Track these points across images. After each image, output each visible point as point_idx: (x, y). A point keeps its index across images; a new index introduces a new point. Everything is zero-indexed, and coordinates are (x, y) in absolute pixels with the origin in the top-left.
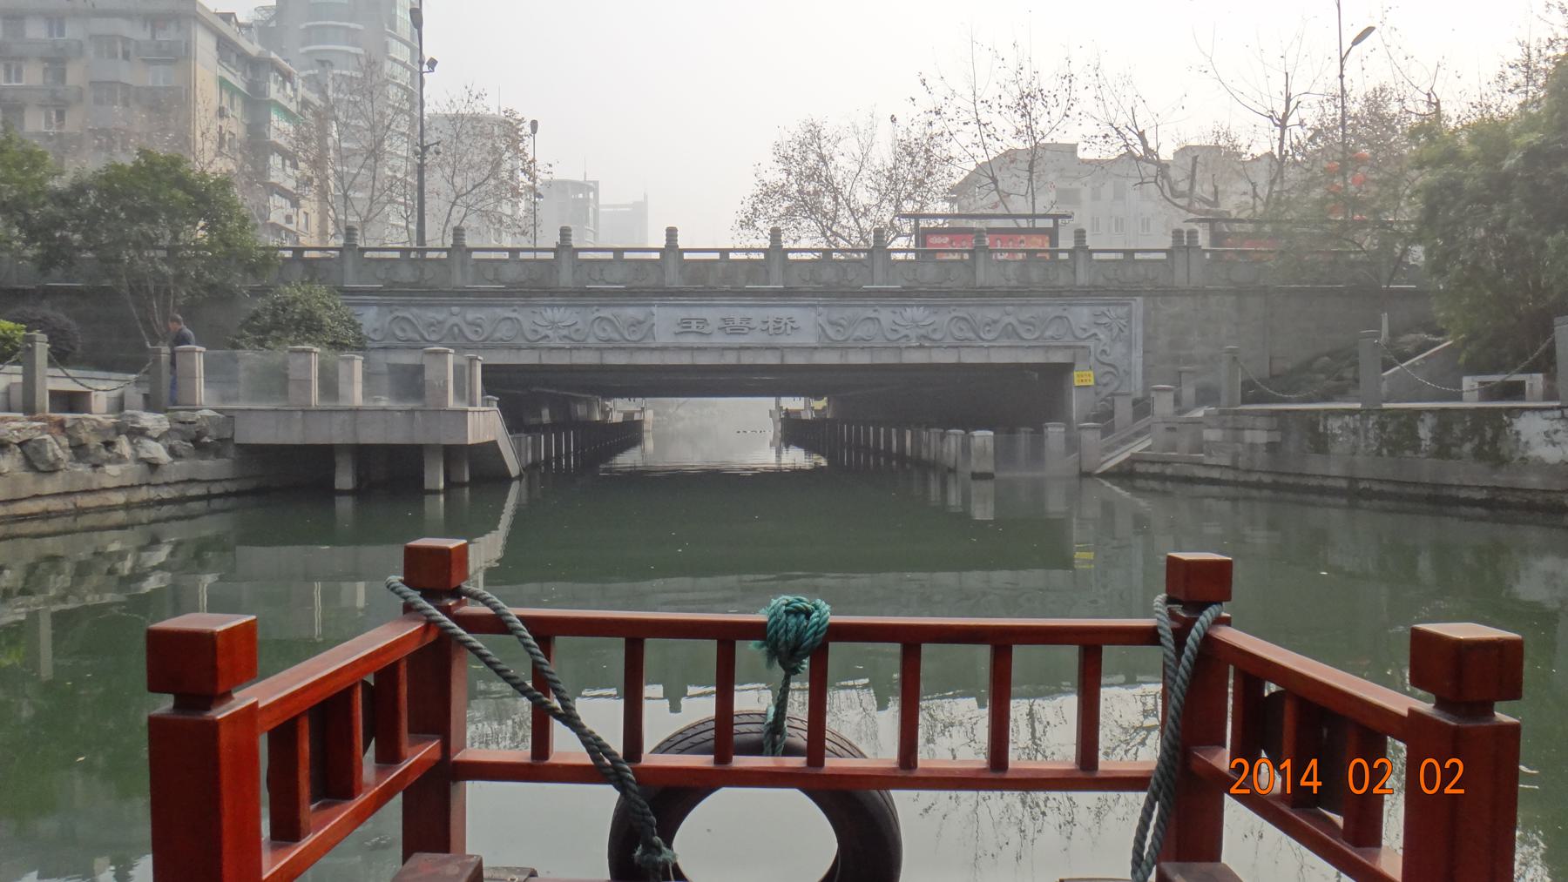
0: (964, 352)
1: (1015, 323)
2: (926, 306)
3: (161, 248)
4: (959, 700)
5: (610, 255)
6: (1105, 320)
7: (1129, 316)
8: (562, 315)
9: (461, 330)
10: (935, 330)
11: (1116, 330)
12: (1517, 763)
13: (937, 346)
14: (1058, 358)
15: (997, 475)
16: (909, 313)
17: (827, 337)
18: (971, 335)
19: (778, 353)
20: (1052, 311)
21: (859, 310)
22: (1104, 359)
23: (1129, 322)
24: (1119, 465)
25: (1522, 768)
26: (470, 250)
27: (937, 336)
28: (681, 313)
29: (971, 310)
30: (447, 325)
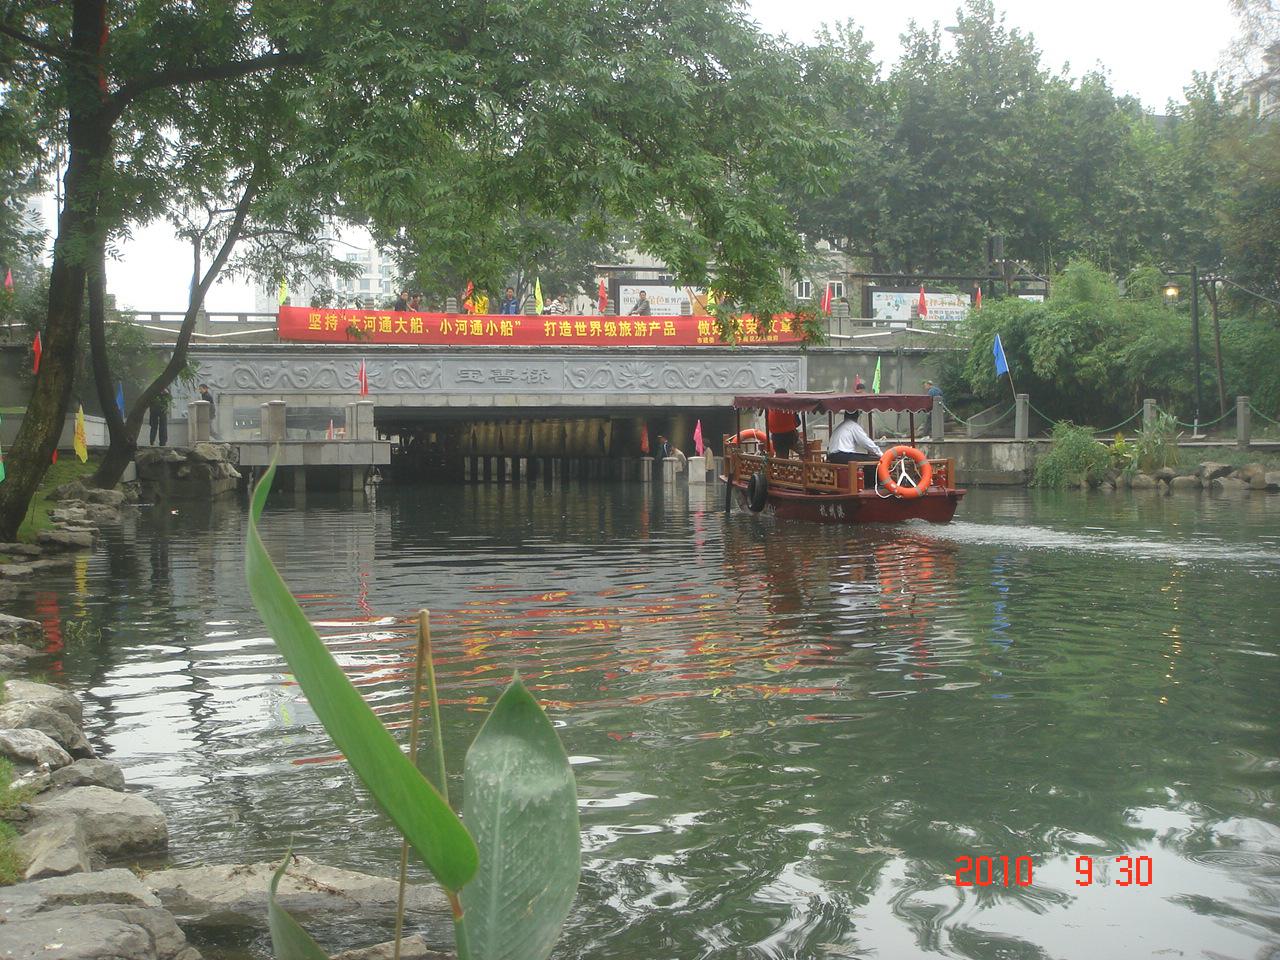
1: (712, 375)
3: (467, 298)
5: (235, 319)
9: (289, 379)
12: (310, 700)
21: (596, 364)
25: (305, 700)
26: (208, 315)
28: (461, 367)
29: (680, 365)
30: (279, 374)
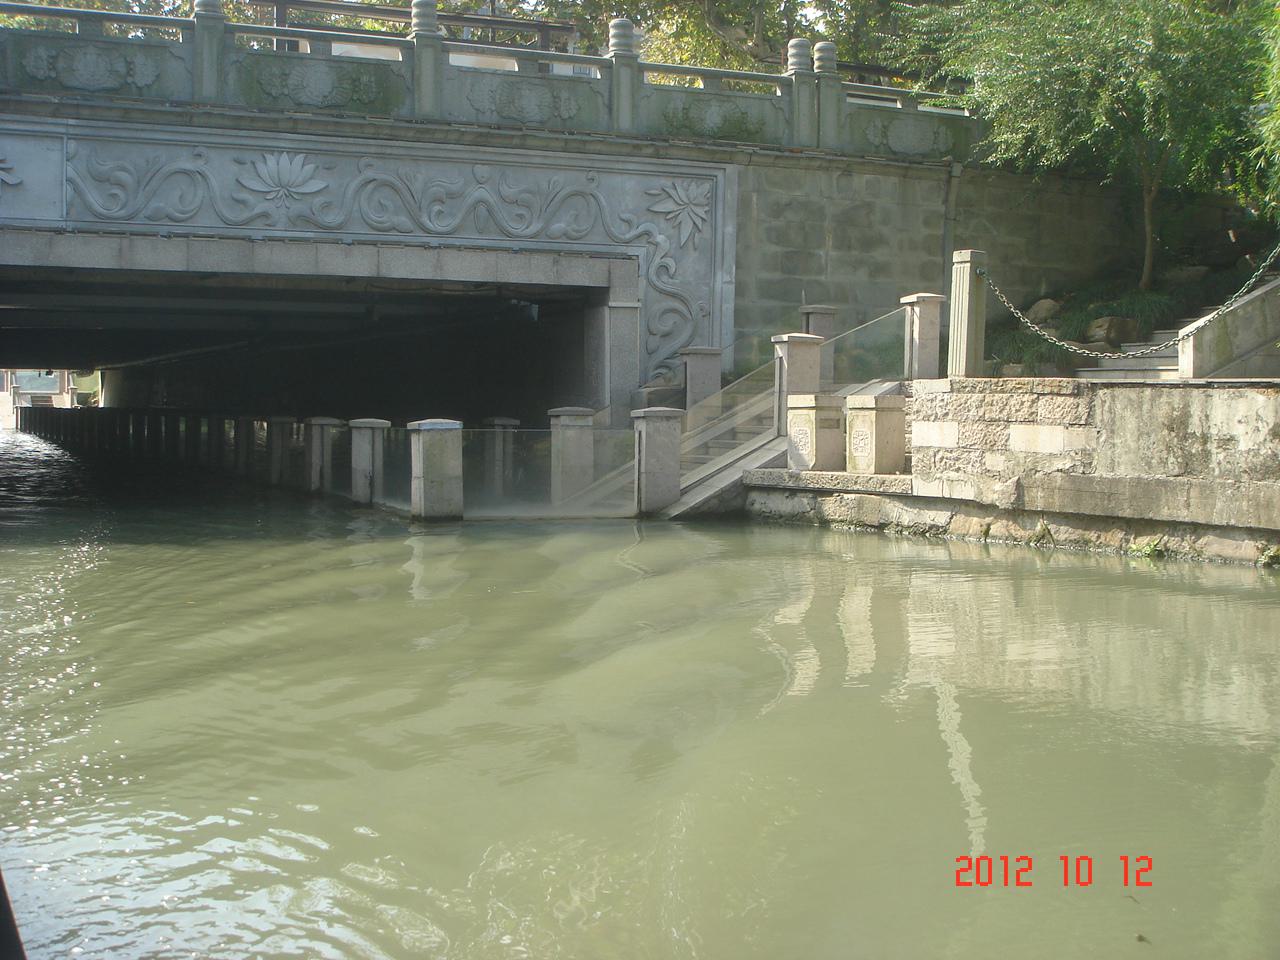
0: (388, 253)
1: (492, 199)
2: (308, 152)
4: (1203, 522)
6: (669, 206)
7: (712, 199)
8: (286, 168)
10: (327, 206)
11: (687, 230)
13: (332, 236)
14: (579, 275)
15: (466, 516)
16: (271, 165)
17: (88, 208)
18: (403, 220)
19: (114, 243)
20: (564, 180)
22: (665, 283)
23: (712, 212)
24: (721, 496)
27: (332, 218)
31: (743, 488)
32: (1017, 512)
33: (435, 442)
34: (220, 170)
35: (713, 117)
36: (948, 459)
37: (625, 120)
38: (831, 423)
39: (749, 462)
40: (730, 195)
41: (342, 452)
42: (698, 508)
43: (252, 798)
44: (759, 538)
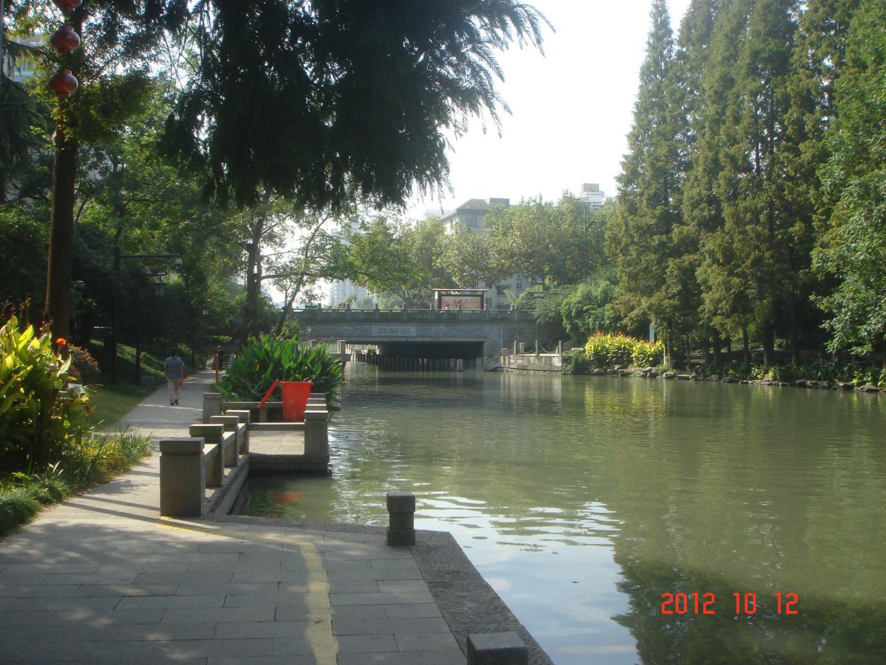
8: (442, 327)
14: (480, 340)
16: (440, 327)
31: (496, 367)
32: (518, 369)
33: (460, 362)
34: (434, 328)
35: (500, 317)
36: (513, 364)
37: (487, 318)
38: (504, 360)
39: (498, 365)
40: (502, 328)
41: (449, 363)
42: (102, 557)
43: (94, 342)
44: (498, 373)
